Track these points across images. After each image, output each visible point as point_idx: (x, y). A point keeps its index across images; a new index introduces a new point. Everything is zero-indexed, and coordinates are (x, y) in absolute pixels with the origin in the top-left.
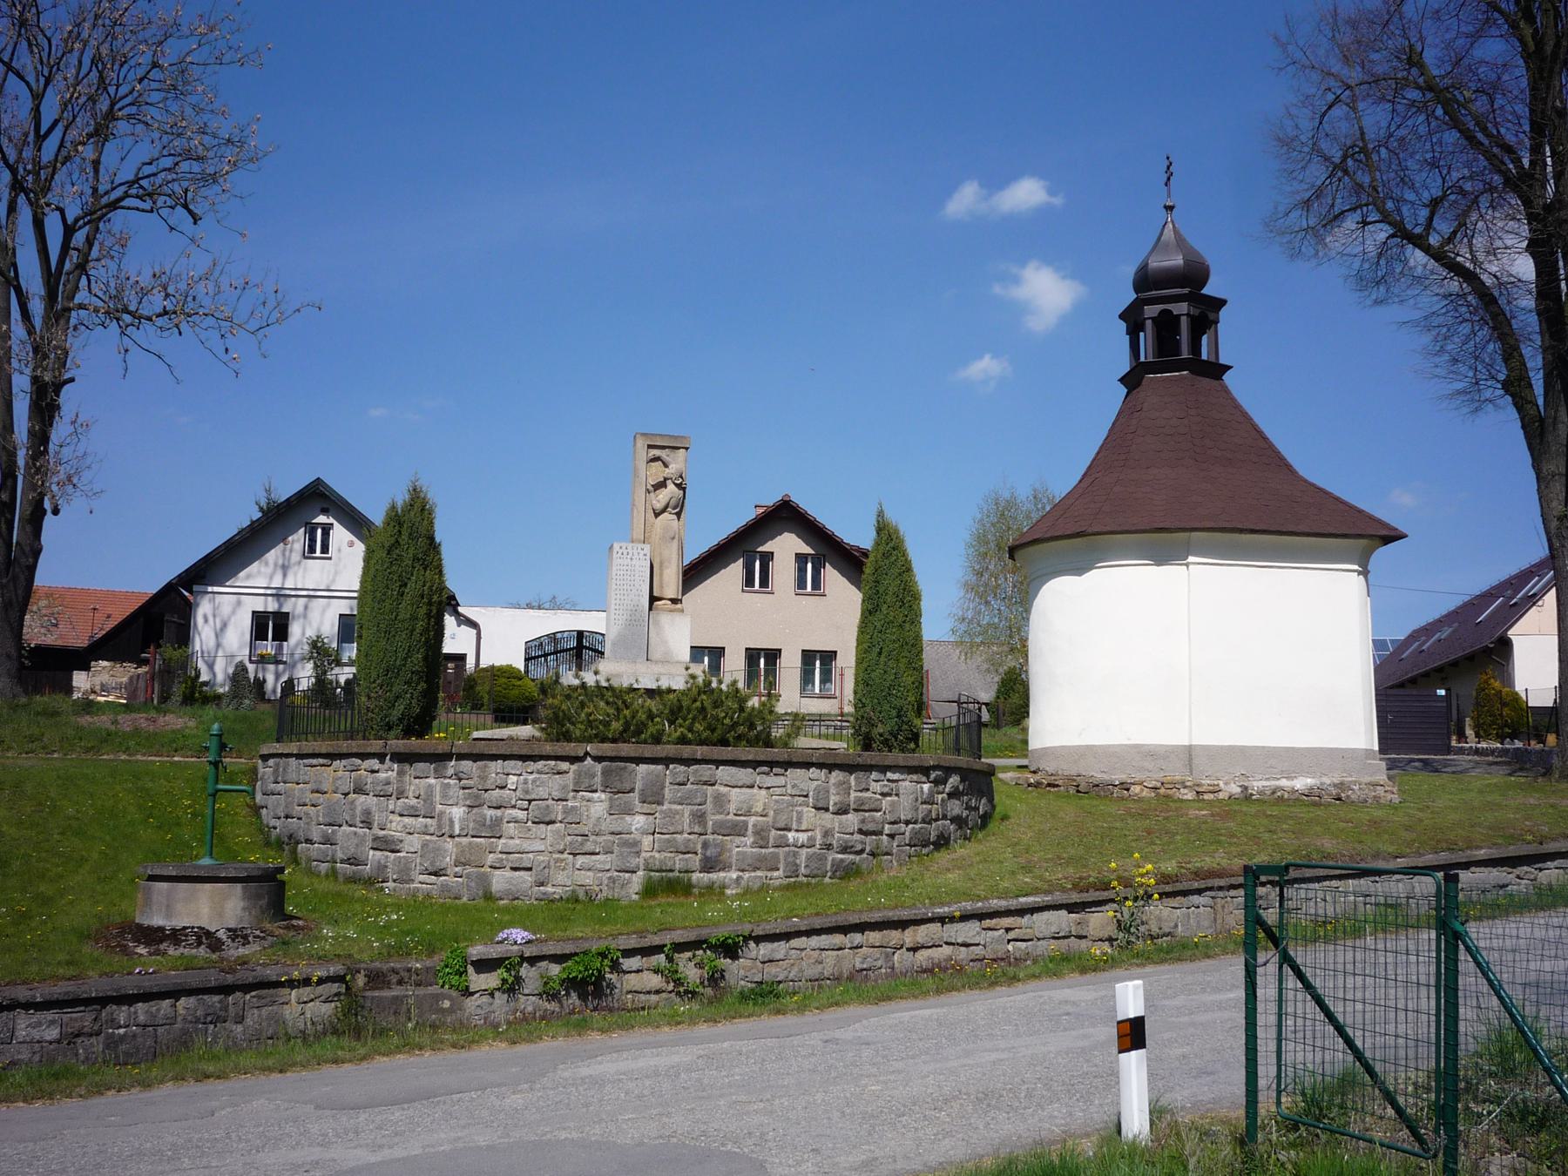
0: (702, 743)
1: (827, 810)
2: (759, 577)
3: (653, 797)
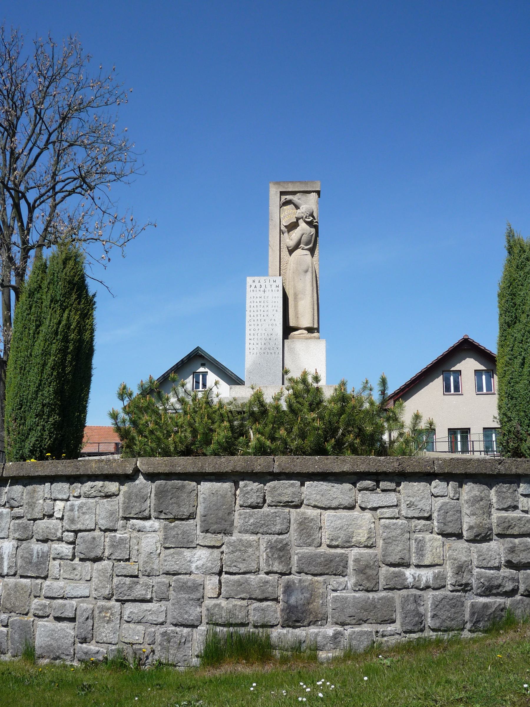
0: (286, 451)
1: (459, 536)
2: (453, 387)
3: (219, 525)
